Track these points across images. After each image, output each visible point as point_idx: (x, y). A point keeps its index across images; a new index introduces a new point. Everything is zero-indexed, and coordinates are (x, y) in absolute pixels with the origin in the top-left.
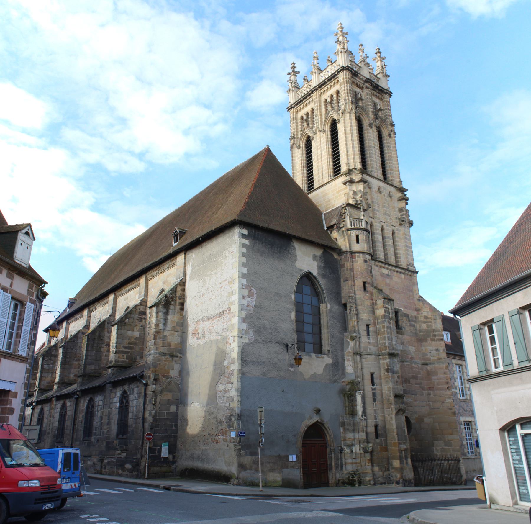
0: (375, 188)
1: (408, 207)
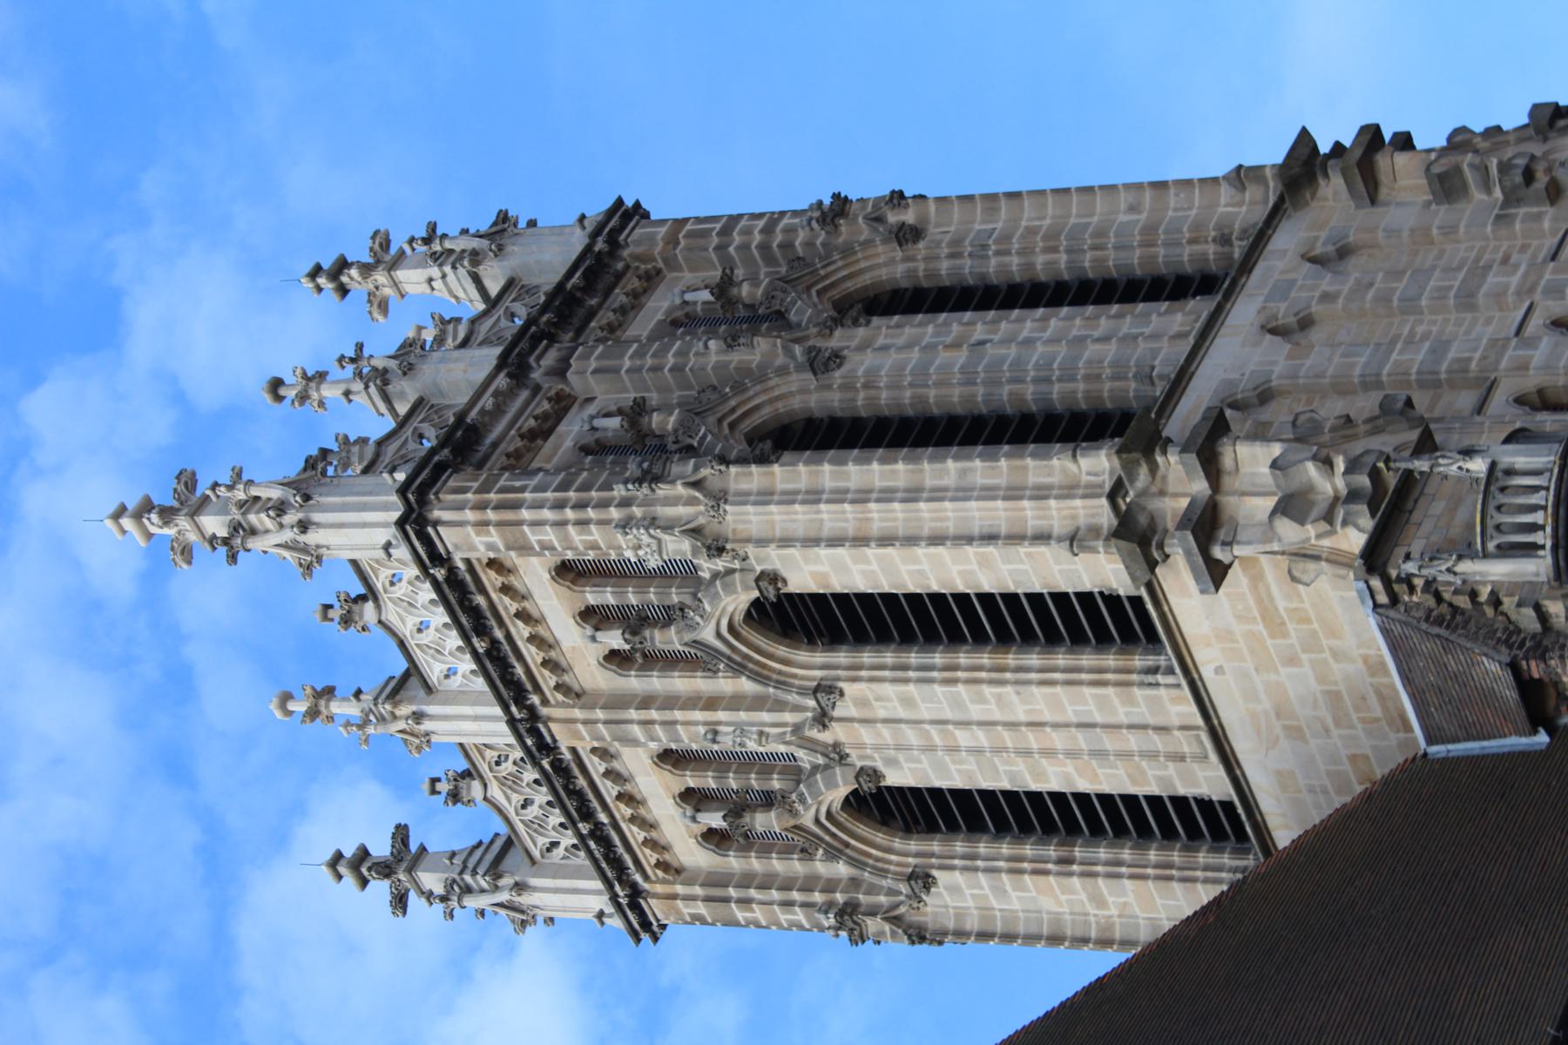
0: (1274, 358)
1: (1430, 137)
